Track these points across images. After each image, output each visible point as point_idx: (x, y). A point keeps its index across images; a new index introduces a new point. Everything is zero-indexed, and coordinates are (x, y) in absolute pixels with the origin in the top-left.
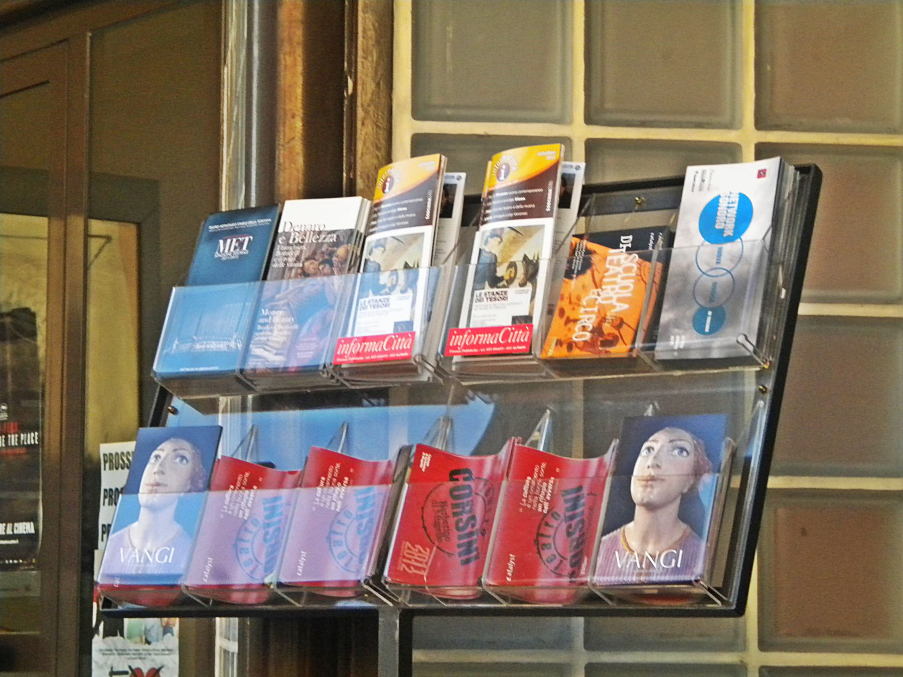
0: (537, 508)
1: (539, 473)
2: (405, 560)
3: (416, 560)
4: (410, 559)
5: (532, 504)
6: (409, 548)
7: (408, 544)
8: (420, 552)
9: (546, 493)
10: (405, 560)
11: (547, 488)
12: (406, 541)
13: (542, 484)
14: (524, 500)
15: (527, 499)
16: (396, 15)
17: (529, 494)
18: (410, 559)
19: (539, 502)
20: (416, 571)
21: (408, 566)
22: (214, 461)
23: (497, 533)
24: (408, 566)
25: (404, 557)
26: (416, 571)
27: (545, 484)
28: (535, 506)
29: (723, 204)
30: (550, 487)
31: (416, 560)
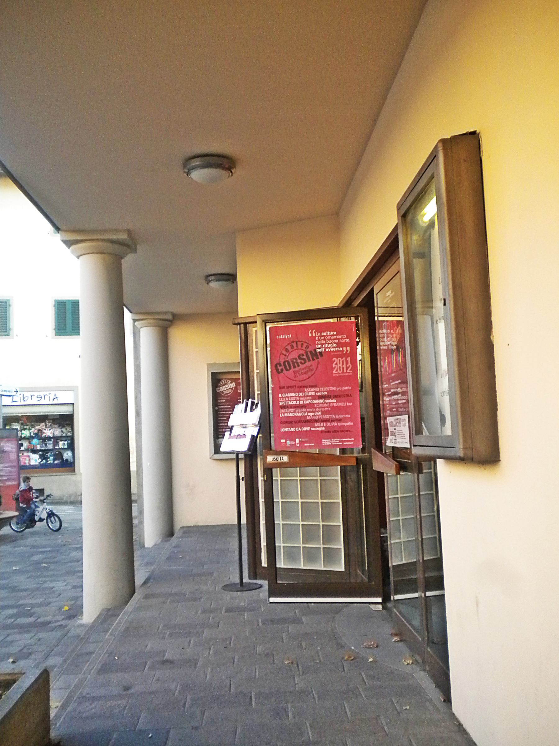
0: (318, 344)
1: (341, 339)
2: (345, 371)
3: (343, 364)
4: (343, 368)
5: (319, 340)
6: (337, 371)
7: (334, 372)
8: (336, 364)
9: (330, 348)
10: (345, 371)
11: (334, 347)
12: (332, 373)
13: (335, 343)
14: (319, 334)
15: (321, 336)
16: (172, 422)
17: (324, 336)
18: (343, 368)
19: (322, 344)
20: (349, 362)
21: (347, 368)
22: (329, 432)
23: (366, 291)
24: (347, 368)
25: (343, 372)
26: (349, 362)
27: (335, 345)
28: (319, 342)
29: (66, 239)
30: (334, 349)
31: (343, 364)
